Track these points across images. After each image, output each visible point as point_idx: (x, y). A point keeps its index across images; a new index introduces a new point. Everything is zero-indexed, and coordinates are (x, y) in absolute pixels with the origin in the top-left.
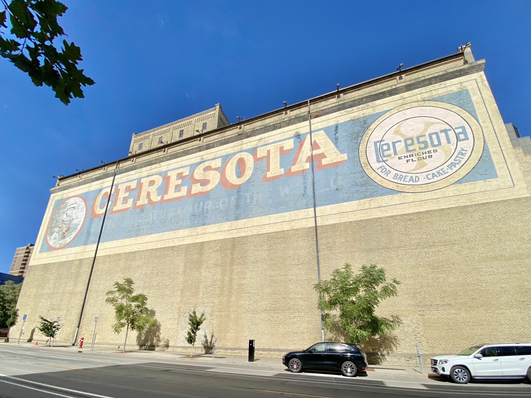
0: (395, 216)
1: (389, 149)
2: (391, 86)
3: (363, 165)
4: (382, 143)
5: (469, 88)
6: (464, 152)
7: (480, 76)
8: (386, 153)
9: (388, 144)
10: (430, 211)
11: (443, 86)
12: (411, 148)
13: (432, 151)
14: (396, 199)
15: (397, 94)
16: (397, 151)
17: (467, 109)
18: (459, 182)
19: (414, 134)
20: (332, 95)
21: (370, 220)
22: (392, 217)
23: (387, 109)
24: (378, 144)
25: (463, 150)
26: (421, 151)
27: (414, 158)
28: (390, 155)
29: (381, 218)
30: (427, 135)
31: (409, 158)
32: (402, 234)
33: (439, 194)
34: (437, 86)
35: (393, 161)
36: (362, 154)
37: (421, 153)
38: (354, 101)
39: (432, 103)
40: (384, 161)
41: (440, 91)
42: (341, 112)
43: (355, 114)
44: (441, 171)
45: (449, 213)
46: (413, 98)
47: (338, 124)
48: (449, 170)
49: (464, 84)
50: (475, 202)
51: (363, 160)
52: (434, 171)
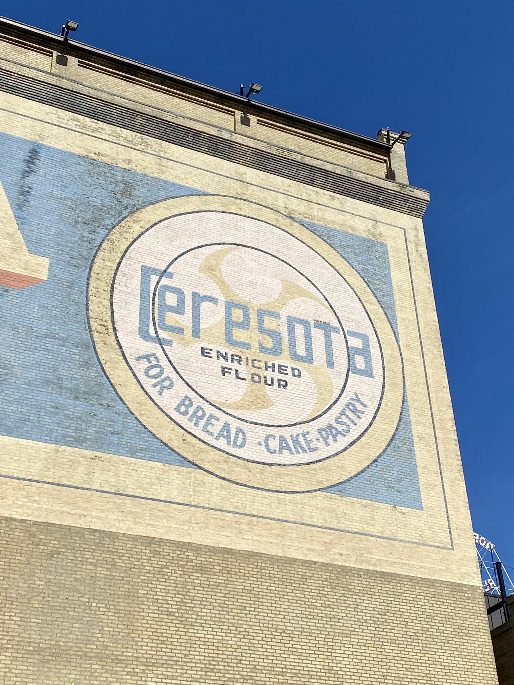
0: (161, 541)
1: (179, 310)
2: (220, 128)
3: (94, 325)
4: (165, 281)
5: (390, 244)
6: (359, 407)
7: (413, 225)
8: (172, 318)
9: (179, 292)
10: (260, 555)
11: (336, 204)
12: (239, 335)
13: (289, 371)
14: (173, 482)
15: (230, 159)
16: (202, 326)
17: (378, 293)
18: (338, 488)
19: (256, 301)
20: (43, 44)
21: (80, 532)
22: (149, 541)
23: (197, 186)
24: (154, 279)
25: (358, 400)
26: (263, 357)
27: (244, 371)
28: (180, 331)
29: (113, 536)
30: (284, 319)
31: (228, 364)
32: (170, 614)
33: (285, 508)
34: (324, 196)
35: (184, 352)
36: (98, 285)
37: (262, 364)
38: (109, 104)
39: (307, 236)
40: (161, 342)
41: (330, 216)
42: (61, 112)
43: (104, 147)
44: (301, 439)
45: (304, 579)
46: (267, 193)
47: (40, 146)
48: (321, 445)
49: (381, 228)
50: (369, 563)
51: (98, 307)
52: (287, 433)
